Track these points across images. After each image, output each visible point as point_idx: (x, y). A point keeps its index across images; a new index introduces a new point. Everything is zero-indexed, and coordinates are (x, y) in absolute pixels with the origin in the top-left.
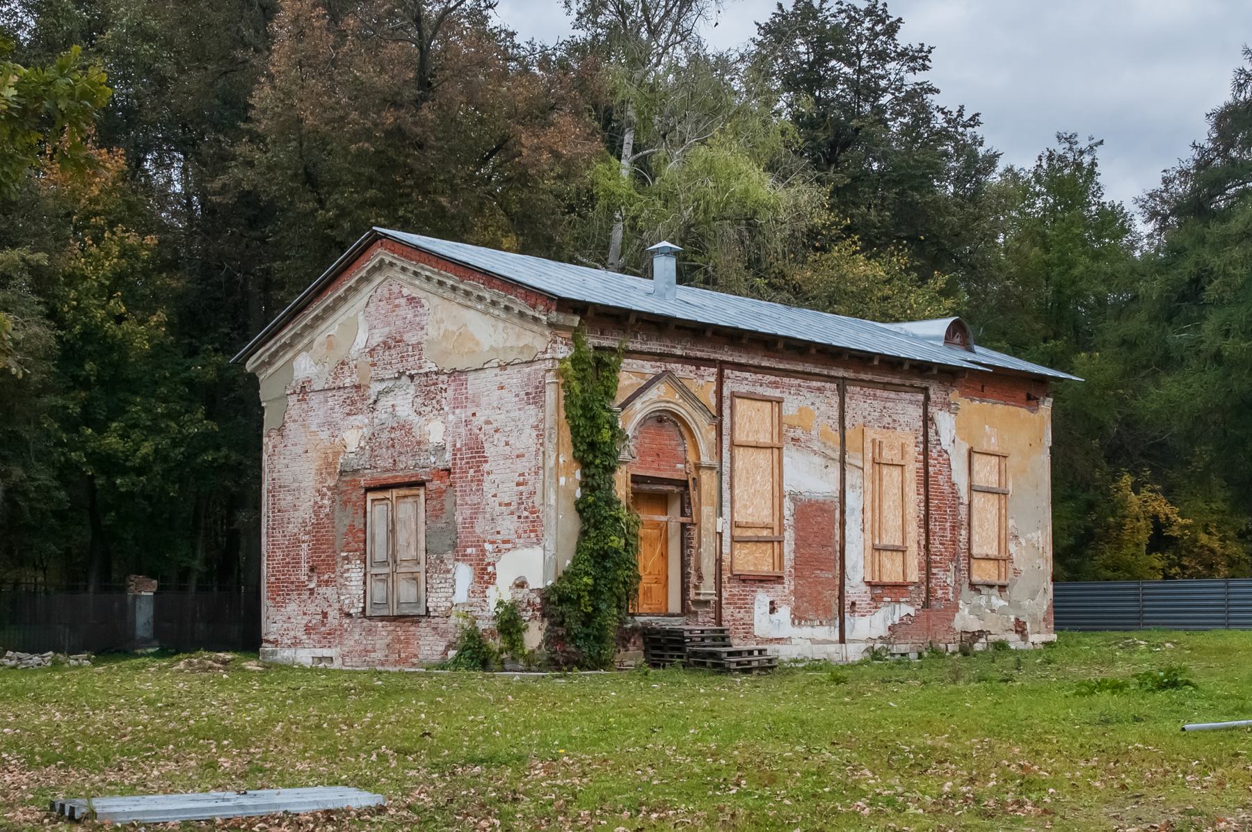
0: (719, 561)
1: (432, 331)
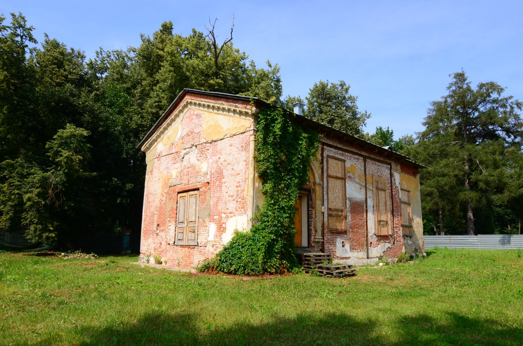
0: (323, 224)
1: (204, 126)
